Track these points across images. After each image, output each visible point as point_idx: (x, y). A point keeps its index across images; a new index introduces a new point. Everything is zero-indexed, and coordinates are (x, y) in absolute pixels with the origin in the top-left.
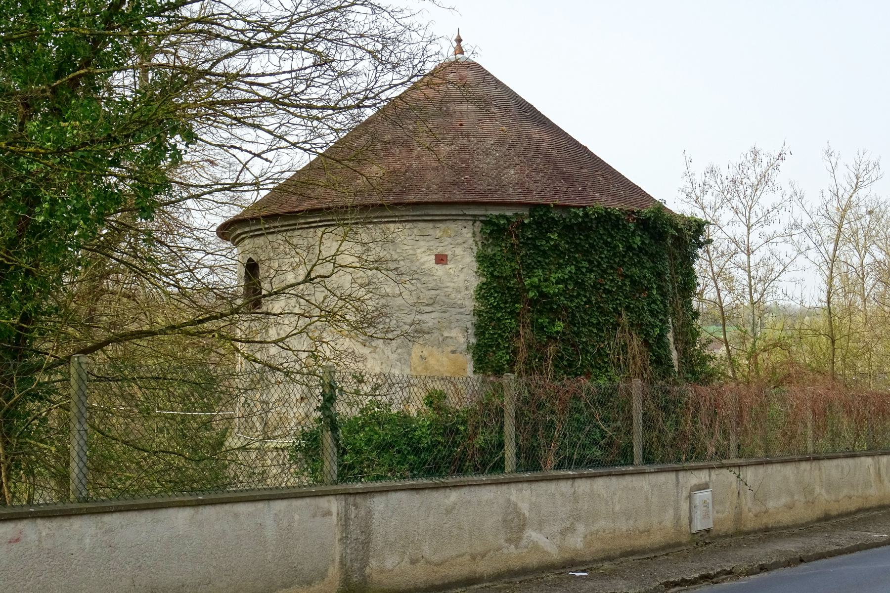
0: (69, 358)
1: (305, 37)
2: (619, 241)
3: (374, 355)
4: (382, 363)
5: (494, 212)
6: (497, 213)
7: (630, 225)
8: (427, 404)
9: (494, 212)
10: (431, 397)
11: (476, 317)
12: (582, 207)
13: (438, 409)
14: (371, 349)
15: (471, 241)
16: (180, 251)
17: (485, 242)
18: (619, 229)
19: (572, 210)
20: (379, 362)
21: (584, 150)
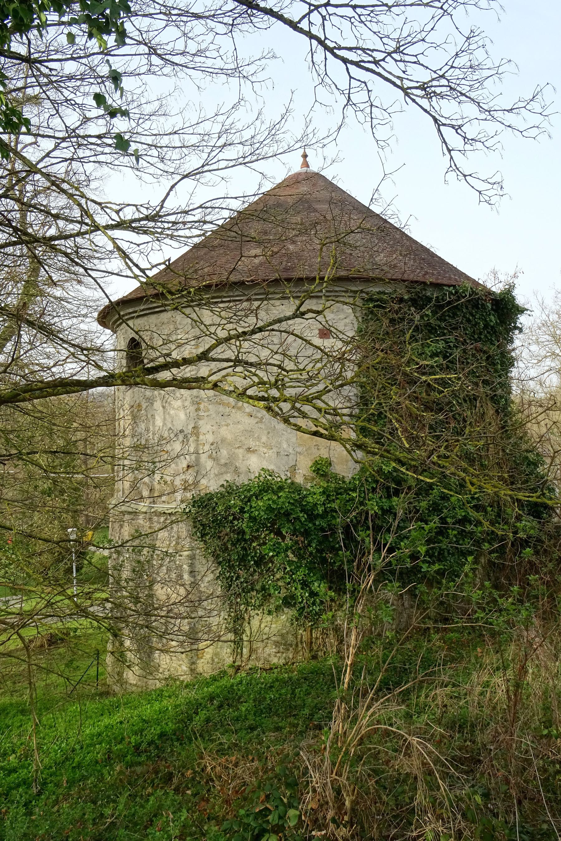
0: (349, 628)
1: (119, 314)
2: (479, 319)
3: (260, 425)
4: (269, 433)
5: (374, 289)
6: (377, 290)
7: (488, 304)
8: (314, 471)
9: (374, 289)
10: (319, 464)
11: (359, 388)
12: (452, 286)
13: (324, 476)
14: (257, 420)
15: (352, 316)
16: (49, 604)
17: (365, 317)
18: (478, 308)
19: (445, 288)
20: (266, 432)
21: (426, 251)
